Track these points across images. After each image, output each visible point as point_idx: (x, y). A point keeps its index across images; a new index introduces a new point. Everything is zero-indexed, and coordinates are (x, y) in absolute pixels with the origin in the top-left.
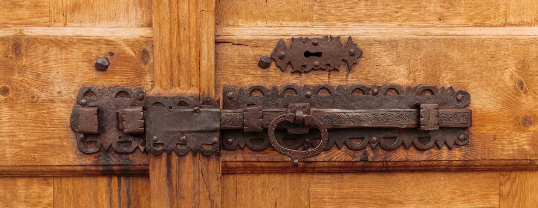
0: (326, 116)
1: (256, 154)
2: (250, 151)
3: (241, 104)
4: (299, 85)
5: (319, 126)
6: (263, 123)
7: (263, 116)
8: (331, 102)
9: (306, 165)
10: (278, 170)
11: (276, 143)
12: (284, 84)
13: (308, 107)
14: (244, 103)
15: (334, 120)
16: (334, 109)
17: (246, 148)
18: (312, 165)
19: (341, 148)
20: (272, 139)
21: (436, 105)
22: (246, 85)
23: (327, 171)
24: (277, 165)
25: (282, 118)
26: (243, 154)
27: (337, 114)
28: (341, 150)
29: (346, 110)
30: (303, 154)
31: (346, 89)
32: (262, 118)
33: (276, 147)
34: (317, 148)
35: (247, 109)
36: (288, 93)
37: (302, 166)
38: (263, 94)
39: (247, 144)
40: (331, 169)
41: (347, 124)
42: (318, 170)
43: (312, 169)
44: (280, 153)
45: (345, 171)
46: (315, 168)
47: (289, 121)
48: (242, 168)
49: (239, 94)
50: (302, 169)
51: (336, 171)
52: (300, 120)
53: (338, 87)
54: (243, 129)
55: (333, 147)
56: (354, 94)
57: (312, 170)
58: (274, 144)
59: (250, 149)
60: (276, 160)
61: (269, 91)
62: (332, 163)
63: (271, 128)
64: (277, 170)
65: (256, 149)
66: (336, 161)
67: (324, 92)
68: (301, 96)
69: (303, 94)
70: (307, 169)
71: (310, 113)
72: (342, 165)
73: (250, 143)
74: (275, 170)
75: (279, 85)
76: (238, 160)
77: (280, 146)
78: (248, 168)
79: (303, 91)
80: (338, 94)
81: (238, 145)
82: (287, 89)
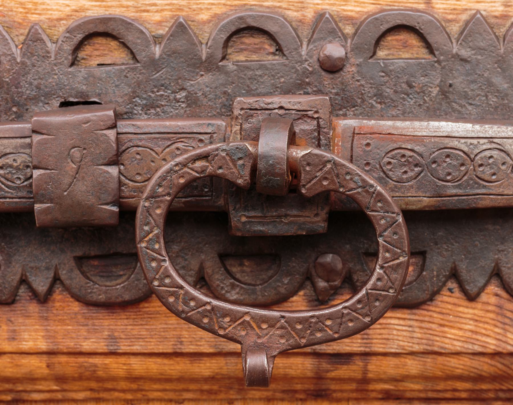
0: (408, 153)
1: (106, 323)
2: (76, 307)
3: (35, 99)
4: (292, 14)
5: (364, 200)
6: (120, 182)
7: (119, 154)
8: (435, 91)
9: (328, 371)
10: (206, 387)
11: (169, 276)
12: (224, 9)
13: (324, 113)
14: (48, 95)
15: (441, 173)
16: (443, 124)
17: (58, 295)
18: (354, 367)
19: (478, 294)
20: (154, 259)
21: (113, 211)
22: (56, 15)
23: (422, 395)
24: (197, 370)
25: (199, 164)
26: (47, 319)
27: (455, 143)
28: (479, 306)
29: (495, 128)
30: (294, 329)
31: (503, 30)
32: (115, 162)
33: (173, 294)
34: (359, 301)
35: (47, 125)
36: (242, 50)
37: (309, 374)
38: (132, 53)
39: (63, 274)
40: (439, 388)
41: (500, 191)
42: (382, 391)
43: (354, 386)
44: (189, 320)
45: (501, 395)
46: (365, 381)
47: (229, 177)
48: (45, 379)
49: (24, 55)
50: (312, 387)
51: (464, 395)
52: (278, 175)
53: (467, 23)
54: (30, 213)
55: (445, 292)
56: (381, 53)
57: (357, 390)
58: (161, 280)
59: (78, 298)
60: (192, 349)
61: (157, 39)
62: (440, 359)
63: (148, 210)
64: (202, 391)
65: (102, 298)
66: (458, 354)
67: (406, 46)
68: (302, 62)
69: (309, 54)
70: (333, 387)
71: (329, 140)
72: (486, 368)
73: (77, 272)
74: (192, 387)
75: (204, 16)
76: (27, 345)
77: (187, 293)
78: (74, 379)
79: (309, 41)
80: (465, 53)
81: (23, 281)
82: (238, 32)
